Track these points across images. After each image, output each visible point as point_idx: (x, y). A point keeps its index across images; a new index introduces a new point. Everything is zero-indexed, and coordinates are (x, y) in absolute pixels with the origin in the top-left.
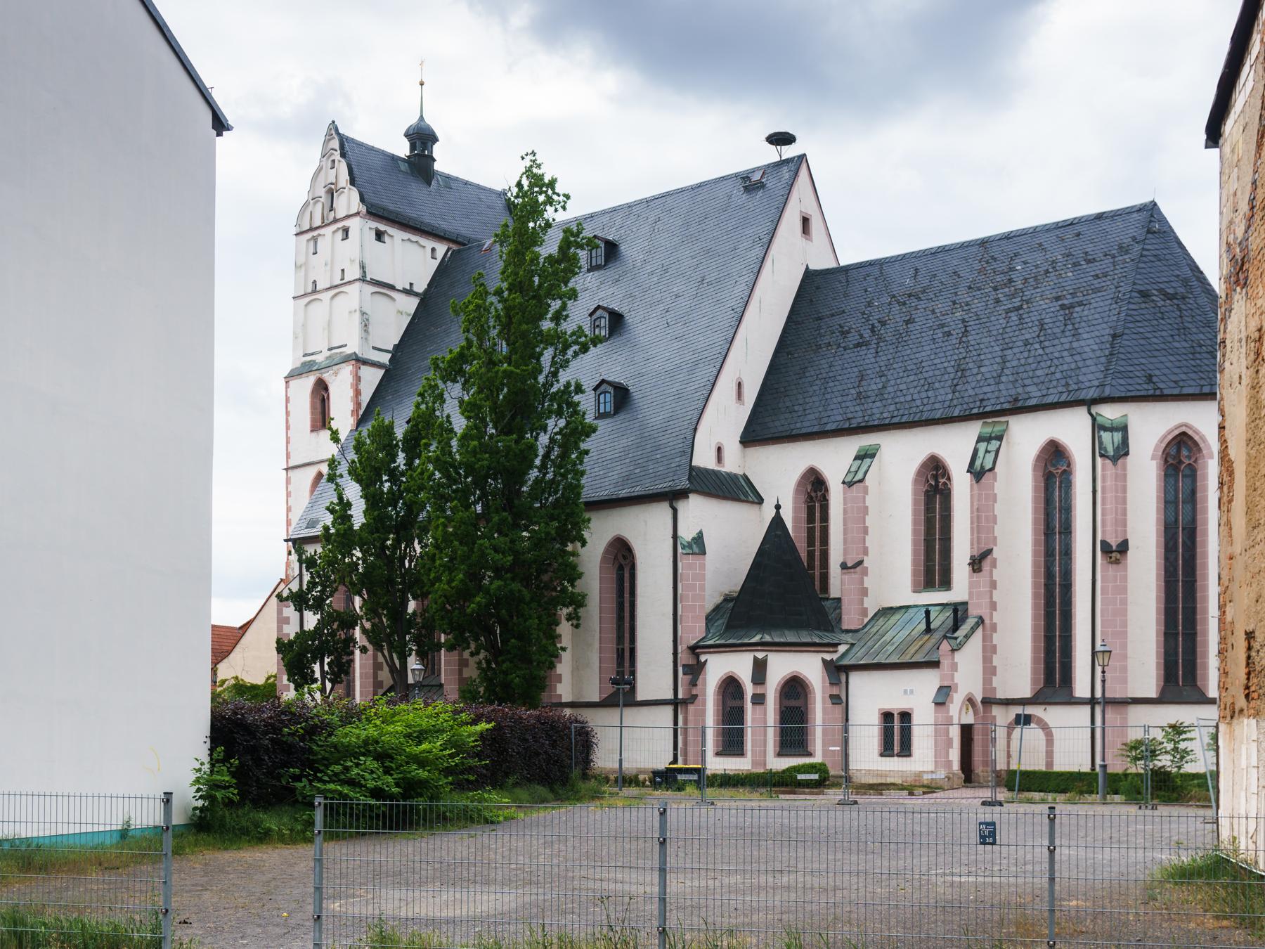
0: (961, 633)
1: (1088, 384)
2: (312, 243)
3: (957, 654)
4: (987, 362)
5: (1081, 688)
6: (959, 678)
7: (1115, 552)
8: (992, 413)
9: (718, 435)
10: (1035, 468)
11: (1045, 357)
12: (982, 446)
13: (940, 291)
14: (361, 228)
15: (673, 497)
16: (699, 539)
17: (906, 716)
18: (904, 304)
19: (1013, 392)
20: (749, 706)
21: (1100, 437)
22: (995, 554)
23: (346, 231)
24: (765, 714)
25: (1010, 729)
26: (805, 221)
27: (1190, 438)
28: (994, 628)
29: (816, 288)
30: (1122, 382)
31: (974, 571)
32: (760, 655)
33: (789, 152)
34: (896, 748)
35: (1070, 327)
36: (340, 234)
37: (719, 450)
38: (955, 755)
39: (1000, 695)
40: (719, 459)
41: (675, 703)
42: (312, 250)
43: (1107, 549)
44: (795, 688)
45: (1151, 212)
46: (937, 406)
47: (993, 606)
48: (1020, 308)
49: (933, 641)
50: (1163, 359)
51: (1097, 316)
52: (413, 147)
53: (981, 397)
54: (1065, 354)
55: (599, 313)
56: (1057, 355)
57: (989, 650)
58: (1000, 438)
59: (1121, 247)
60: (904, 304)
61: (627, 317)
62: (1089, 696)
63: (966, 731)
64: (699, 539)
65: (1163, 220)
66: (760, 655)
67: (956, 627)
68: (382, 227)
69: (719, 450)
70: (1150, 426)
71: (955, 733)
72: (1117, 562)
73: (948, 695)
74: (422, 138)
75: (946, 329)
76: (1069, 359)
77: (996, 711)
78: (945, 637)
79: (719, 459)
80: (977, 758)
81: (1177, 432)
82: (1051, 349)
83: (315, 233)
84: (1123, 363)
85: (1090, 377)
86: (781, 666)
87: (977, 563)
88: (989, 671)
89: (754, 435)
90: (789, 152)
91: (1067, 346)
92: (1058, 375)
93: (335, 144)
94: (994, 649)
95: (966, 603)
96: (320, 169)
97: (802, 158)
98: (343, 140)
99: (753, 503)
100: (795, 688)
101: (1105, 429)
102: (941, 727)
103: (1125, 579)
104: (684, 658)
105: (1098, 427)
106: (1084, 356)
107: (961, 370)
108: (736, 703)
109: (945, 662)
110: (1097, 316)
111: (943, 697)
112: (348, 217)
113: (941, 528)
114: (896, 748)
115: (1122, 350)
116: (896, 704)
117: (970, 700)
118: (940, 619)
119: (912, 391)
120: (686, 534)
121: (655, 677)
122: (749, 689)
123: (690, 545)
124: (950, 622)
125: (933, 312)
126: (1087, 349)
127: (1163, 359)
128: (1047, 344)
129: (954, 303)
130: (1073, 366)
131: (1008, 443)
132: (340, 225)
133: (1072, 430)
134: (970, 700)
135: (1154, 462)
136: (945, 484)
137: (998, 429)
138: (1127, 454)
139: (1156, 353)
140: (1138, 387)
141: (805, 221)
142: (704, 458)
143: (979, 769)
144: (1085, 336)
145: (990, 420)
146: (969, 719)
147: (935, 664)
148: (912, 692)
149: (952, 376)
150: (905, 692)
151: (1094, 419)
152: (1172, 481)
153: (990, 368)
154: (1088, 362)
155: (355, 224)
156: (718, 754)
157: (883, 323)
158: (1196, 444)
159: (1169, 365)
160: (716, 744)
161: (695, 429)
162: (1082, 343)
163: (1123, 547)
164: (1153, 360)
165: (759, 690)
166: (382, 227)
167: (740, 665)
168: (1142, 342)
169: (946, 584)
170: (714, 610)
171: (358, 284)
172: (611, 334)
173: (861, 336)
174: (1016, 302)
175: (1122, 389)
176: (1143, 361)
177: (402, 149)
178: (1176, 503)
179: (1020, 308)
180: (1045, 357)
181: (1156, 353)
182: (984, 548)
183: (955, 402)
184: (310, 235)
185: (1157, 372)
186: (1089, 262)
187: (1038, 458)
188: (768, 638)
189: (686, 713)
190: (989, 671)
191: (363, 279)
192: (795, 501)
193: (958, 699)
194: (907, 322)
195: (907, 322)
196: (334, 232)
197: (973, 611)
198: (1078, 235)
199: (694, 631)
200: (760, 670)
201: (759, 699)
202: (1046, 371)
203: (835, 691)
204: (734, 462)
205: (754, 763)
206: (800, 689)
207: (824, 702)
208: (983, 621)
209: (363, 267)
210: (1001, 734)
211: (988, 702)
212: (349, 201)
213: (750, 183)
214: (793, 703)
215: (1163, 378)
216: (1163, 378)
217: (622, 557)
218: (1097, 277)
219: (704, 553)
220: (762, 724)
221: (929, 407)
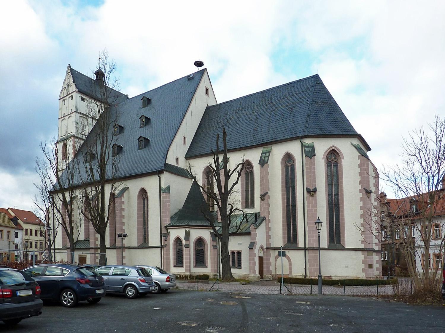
0: (257, 223)
1: (300, 131)
2: (63, 102)
3: (257, 230)
4: (264, 128)
5: (301, 244)
6: (257, 239)
7: (312, 192)
8: (266, 144)
9: (177, 154)
10: (282, 163)
11: (284, 124)
12: (264, 155)
13: (248, 108)
14: (77, 96)
15: (159, 173)
16: (168, 188)
17: (239, 253)
18: (237, 113)
19: (273, 136)
20: (184, 248)
21: (305, 150)
22: (269, 194)
23: (72, 97)
24: (190, 251)
25: (276, 258)
26: (207, 90)
27: (336, 151)
28: (269, 221)
29: (209, 110)
30: (311, 130)
31: (262, 200)
32: (188, 230)
33: (201, 68)
34: (236, 265)
35: (292, 114)
36: (71, 98)
37: (177, 159)
38: (257, 268)
39: (272, 246)
40: (177, 162)
41: (161, 247)
42: (63, 104)
43: (309, 191)
44: (200, 242)
45: (316, 79)
46: (248, 142)
47: (269, 213)
48: (275, 110)
49: (248, 225)
50: (325, 123)
51: (301, 110)
52: (97, 77)
53: (262, 139)
54: (291, 122)
55: (142, 118)
56: (288, 123)
57: (268, 229)
58: (269, 152)
59: (307, 89)
60: (237, 113)
61: (151, 120)
62: (304, 247)
63: (261, 259)
64: (168, 188)
65: (320, 80)
66: (188, 230)
67: (256, 220)
68: (84, 97)
69: (177, 159)
70: (322, 147)
71: (257, 260)
72: (313, 196)
73: (253, 245)
74: (100, 74)
75: (250, 119)
76: (292, 124)
77: (271, 252)
78: (252, 223)
79: (177, 162)
80: (265, 270)
81: (331, 149)
82: (286, 122)
83: (64, 99)
84: (311, 124)
85: (300, 129)
86: (195, 234)
87: (263, 197)
88: (268, 237)
89: (189, 156)
90: (201, 68)
91: (291, 120)
92: (289, 130)
93: (69, 71)
94: (269, 229)
95: (260, 213)
96: (65, 79)
97: (205, 69)
98: (72, 70)
99: (189, 178)
100: (200, 242)
101: (306, 147)
102: (251, 259)
103: (316, 202)
104: (164, 231)
105: (303, 146)
106: (298, 123)
107: (255, 131)
108: (180, 247)
109: (252, 233)
110: (301, 110)
111: (252, 246)
112: (72, 92)
113: (251, 195)
114: (236, 265)
115: (310, 120)
116: (36, 237)
117: (262, 248)
118: (251, 219)
119: (240, 138)
120: (163, 186)
121: (154, 239)
122: (184, 242)
123: (164, 190)
124: (254, 219)
125: (246, 114)
126: (298, 120)
127: (325, 123)
128: (284, 120)
129: (253, 111)
130: (294, 126)
131: (272, 154)
132: (70, 95)
133: (294, 148)
134: (262, 248)
135: (324, 160)
136: (251, 170)
137: (269, 149)
138: (315, 155)
139: (322, 121)
140: (317, 132)
141: (207, 90)
142: (171, 161)
143: (266, 274)
144: (298, 116)
145: (265, 147)
146: (262, 255)
147: (249, 234)
148: (241, 244)
149: (253, 133)
150: (239, 244)
151: (302, 144)
152: (329, 168)
153: (265, 129)
154: (299, 125)
155: (74, 94)
156: (174, 266)
157: (231, 119)
158: (338, 154)
159: (327, 125)
160: (174, 263)
161: (168, 151)
162: (297, 119)
163: (315, 191)
164: (321, 123)
165: (187, 242)
166: (84, 97)
167: (180, 233)
168: (318, 117)
169: (253, 206)
170: (175, 214)
171: (75, 113)
172: (146, 125)
173: (224, 123)
174: (274, 108)
175: (312, 132)
176: (318, 124)
177: (94, 78)
178: (331, 175)
179: (275, 110)
180: (284, 124)
181: (322, 121)
182: (265, 191)
183: (254, 141)
184: (62, 100)
185: (323, 127)
186: (297, 94)
187: (283, 160)
188: (190, 224)
189: (163, 250)
190: (268, 237)
191: (77, 112)
192: (203, 178)
193: (257, 247)
194: (238, 118)
195: (238, 118)
196: (69, 98)
197: (262, 215)
198: (293, 87)
199: (167, 221)
200: (187, 234)
201: (187, 246)
202: (285, 129)
203: (215, 244)
204: (183, 164)
205: (186, 270)
206: (202, 243)
207: (211, 248)
208: (265, 219)
209: (77, 108)
210: (272, 259)
211: (267, 248)
212: (73, 88)
213: (189, 78)
214: (200, 248)
215: (326, 129)
216: (326, 129)
217: (343, 287)
218: (300, 98)
219: (170, 193)
220: (189, 255)
221: (245, 143)
